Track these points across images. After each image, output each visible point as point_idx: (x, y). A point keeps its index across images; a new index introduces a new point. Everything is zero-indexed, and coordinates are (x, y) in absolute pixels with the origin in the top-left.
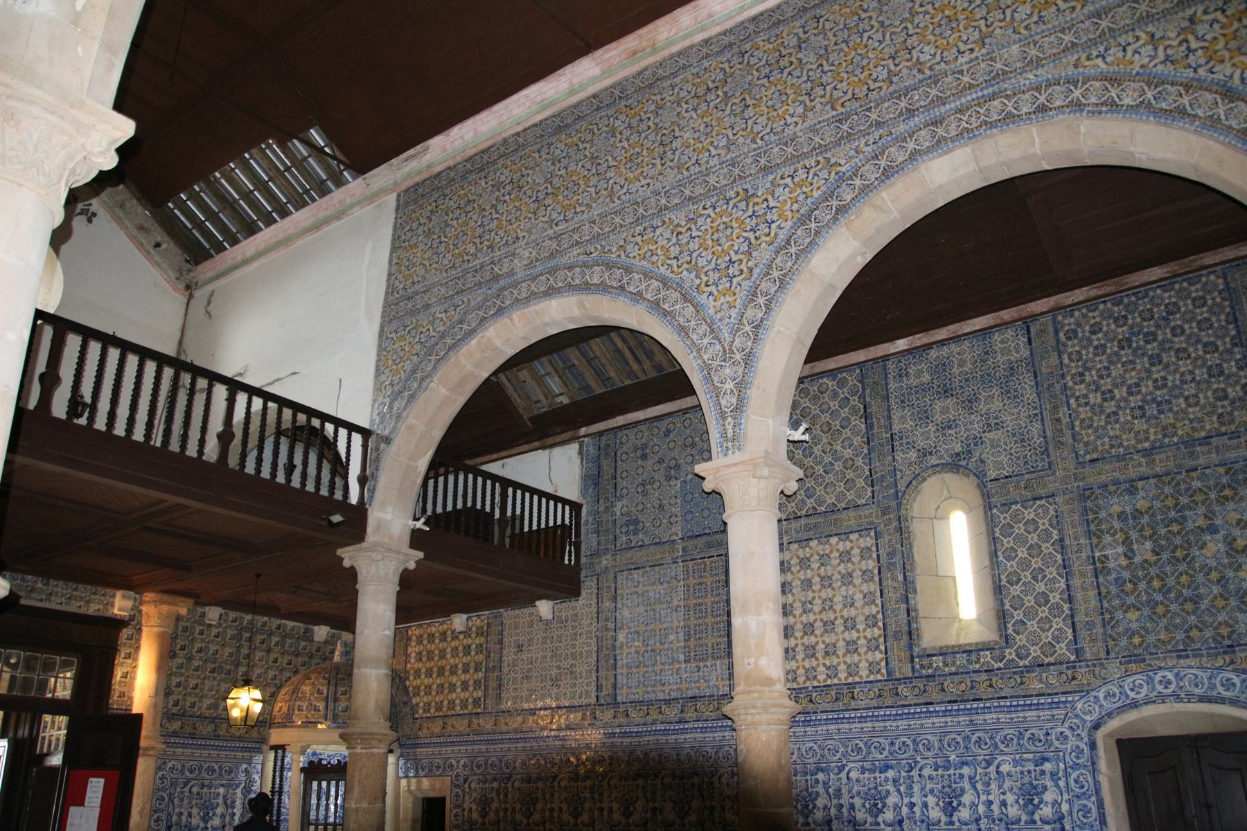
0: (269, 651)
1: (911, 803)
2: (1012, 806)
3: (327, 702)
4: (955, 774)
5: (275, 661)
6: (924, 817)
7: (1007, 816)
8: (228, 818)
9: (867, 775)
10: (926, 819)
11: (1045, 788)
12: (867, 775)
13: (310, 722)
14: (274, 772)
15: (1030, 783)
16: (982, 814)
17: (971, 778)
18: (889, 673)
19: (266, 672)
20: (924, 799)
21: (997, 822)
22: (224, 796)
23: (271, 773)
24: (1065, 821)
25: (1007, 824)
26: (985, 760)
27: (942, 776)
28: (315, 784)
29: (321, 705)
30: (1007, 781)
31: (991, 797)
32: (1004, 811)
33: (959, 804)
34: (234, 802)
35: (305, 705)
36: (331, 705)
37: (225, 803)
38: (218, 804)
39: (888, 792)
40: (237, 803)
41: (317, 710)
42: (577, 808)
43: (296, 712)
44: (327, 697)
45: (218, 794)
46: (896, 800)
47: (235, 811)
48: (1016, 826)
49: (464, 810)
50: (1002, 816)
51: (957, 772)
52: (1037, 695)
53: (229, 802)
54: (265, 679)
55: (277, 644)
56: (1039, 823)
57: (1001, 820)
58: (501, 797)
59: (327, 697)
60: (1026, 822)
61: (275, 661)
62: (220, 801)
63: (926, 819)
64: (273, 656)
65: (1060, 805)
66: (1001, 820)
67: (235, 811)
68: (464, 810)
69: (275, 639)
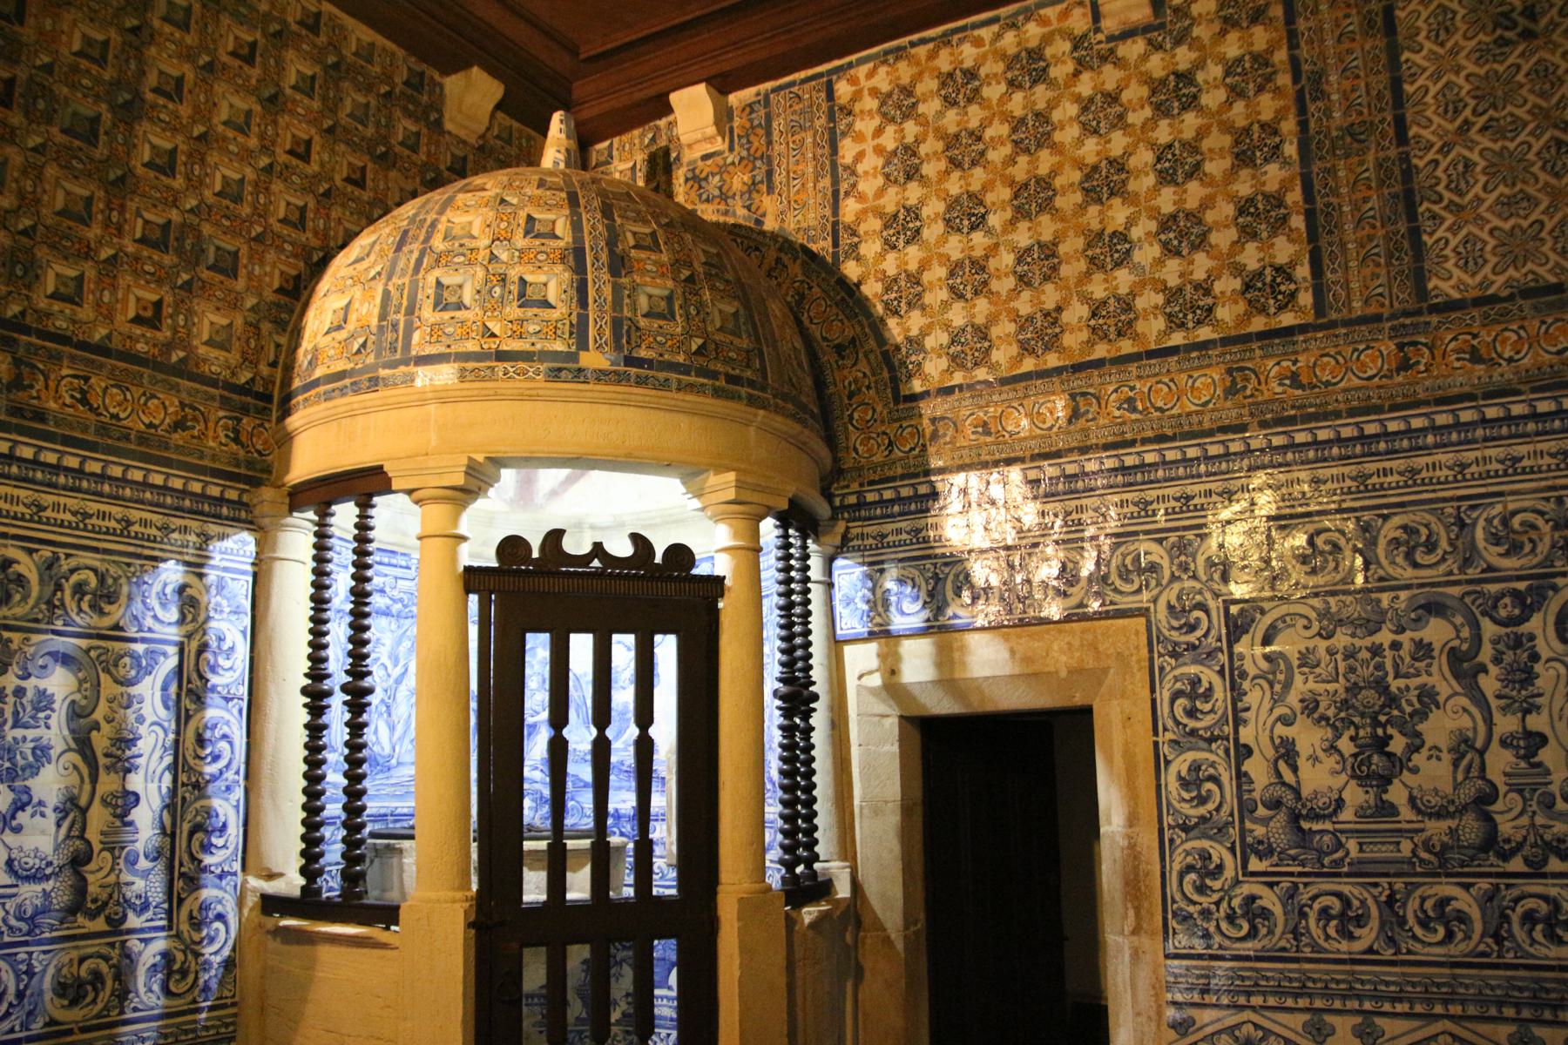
0: (274, 103)
1: (1528, 734)
2: (1314, 759)
3: (579, 268)
4: (1396, 646)
5: (302, 152)
6: (1279, 791)
7: (1296, 791)
8: (98, 817)
9: (1342, 639)
10: (1289, 797)
11: (1428, 698)
12: (1342, 639)
13: (501, 356)
14: (320, 602)
15: (1380, 686)
16: (1499, 781)
17: (1455, 657)
18: (1320, 306)
19: (262, 187)
20: (1280, 730)
21: (1262, 811)
22: (76, 713)
23: (305, 609)
24: (1499, 806)
25: (1295, 818)
26: (1515, 594)
27: (1350, 654)
28: (538, 648)
29: (554, 282)
30: (1298, 679)
31: (1536, 722)
32: (1288, 777)
33: (1414, 749)
34: (124, 742)
35: (468, 282)
36: (600, 282)
37: (83, 744)
38: (42, 752)
39: (1428, 698)
40: (143, 746)
41: (526, 297)
42: (1381, 743)
43: (428, 313)
44: (579, 252)
45: (44, 701)
46: (1466, 722)
47: (135, 782)
48: (1328, 826)
49: (1245, 752)
50: (1279, 791)
51: (1405, 638)
52: (1352, 413)
53: (100, 741)
54: (261, 213)
55: (307, 86)
56: (1406, 813)
57: (1275, 804)
58: (1489, 684)
59: (579, 252)
60: (1361, 813)
61: (302, 152)
62: (56, 732)
63: (1289, 797)
64: (293, 128)
65: (1482, 753)
66: (1275, 804)
67: (135, 782)
68: (1245, 752)
69: (297, 67)
